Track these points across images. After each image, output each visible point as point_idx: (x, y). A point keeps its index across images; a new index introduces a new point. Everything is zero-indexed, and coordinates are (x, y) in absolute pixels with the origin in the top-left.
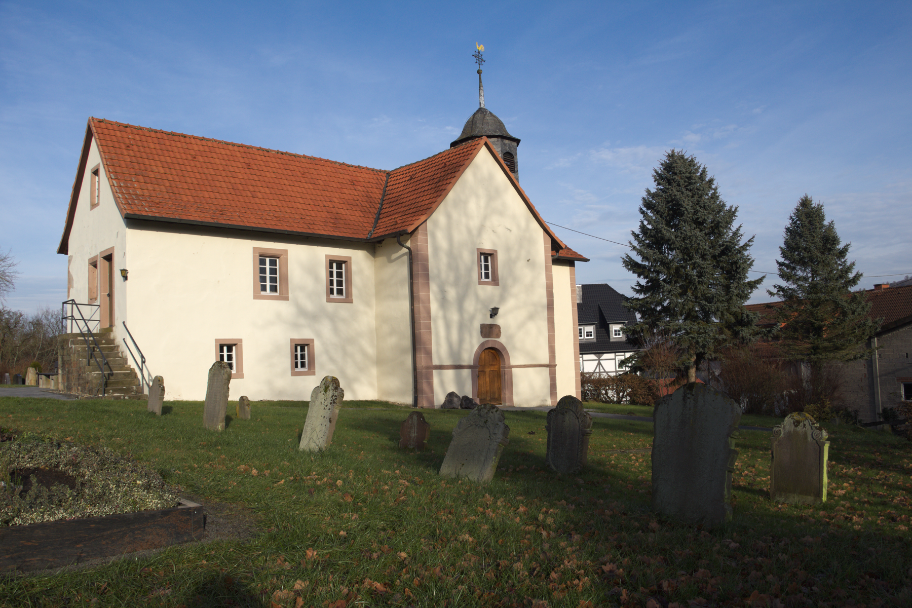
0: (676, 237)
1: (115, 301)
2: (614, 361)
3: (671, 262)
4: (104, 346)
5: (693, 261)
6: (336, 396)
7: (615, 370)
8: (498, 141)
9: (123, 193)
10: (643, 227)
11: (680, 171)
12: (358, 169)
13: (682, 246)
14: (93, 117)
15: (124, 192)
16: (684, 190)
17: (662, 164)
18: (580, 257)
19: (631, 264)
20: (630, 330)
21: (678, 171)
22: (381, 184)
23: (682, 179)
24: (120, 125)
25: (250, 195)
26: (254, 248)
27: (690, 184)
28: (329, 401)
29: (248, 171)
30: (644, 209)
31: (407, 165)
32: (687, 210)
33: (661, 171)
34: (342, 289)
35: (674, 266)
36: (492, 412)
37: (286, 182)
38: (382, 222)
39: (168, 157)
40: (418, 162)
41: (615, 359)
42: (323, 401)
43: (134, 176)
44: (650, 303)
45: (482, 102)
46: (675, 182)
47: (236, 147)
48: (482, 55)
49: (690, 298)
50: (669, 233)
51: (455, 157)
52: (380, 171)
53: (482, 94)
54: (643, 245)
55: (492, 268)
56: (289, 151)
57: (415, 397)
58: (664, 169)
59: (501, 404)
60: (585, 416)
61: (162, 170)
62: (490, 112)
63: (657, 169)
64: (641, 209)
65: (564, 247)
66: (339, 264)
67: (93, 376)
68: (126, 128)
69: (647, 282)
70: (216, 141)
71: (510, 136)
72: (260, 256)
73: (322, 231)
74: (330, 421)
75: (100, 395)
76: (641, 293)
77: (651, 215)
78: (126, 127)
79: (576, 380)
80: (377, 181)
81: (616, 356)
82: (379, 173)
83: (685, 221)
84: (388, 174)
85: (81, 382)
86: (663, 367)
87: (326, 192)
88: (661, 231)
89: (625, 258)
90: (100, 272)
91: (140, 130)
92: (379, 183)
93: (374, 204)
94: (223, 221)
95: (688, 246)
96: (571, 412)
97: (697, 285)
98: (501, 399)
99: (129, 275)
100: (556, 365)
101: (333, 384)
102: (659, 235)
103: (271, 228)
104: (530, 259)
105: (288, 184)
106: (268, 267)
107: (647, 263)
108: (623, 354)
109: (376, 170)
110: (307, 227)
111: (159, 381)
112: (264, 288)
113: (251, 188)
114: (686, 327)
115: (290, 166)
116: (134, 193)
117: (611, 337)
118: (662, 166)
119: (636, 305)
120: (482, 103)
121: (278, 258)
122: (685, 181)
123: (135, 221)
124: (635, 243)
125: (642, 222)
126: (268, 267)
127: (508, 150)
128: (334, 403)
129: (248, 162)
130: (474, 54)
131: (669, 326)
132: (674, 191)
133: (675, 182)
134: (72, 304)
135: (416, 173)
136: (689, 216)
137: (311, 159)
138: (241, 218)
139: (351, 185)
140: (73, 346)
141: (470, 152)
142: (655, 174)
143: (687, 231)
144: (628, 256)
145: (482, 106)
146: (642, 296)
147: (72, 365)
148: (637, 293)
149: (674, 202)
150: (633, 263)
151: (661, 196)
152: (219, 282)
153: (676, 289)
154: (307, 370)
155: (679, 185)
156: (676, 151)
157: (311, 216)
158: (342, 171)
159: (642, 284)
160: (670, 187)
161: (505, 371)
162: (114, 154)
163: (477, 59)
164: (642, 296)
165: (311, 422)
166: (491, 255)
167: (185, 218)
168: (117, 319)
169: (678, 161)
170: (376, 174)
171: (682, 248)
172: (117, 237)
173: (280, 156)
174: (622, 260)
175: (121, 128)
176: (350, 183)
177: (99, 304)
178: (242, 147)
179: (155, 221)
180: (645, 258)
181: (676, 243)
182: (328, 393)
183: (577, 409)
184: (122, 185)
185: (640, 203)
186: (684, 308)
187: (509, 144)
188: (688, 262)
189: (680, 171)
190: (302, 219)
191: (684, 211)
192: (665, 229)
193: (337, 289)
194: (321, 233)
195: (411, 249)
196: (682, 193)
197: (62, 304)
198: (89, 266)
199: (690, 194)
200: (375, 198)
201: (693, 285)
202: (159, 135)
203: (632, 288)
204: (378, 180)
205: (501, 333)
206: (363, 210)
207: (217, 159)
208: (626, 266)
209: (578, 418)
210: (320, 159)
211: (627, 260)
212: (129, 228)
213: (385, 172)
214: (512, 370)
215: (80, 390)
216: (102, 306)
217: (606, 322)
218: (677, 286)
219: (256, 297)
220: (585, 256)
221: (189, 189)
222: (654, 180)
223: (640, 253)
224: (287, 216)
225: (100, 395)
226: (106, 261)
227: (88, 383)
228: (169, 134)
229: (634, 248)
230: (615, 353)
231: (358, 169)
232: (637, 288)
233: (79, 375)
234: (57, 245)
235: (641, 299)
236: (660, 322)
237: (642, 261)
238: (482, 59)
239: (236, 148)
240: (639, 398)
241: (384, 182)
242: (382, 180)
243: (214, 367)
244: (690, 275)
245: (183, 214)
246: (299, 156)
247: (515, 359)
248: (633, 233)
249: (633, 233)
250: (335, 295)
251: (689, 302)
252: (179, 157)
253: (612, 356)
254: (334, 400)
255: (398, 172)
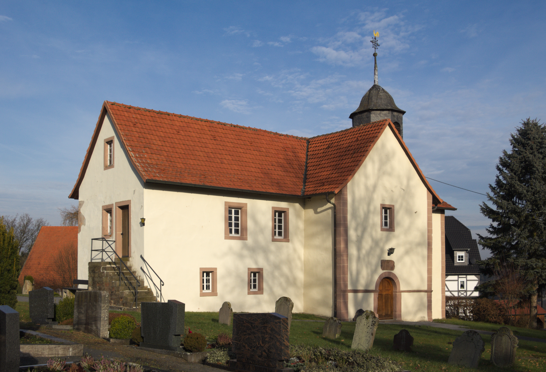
0: (527, 191)
1: (132, 239)
2: (457, 282)
3: (522, 211)
4: (125, 271)
5: (540, 211)
6: (375, 321)
7: (457, 290)
8: (389, 113)
9: (139, 162)
10: (498, 182)
11: (534, 138)
12: (286, 137)
13: (532, 199)
14: (107, 101)
15: (140, 161)
16: (536, 153)
17: (518, 130)
18: (449, 207)
19: (487, 211)
20: (485, 263)
21: (532, 137)
22: (304, 150)
23: (534, 143)
24: (125, 106)
25: (219, 162)
26: (226, 202)
27: (541, 148)
28: (370, 324)
29: (214, 142)
30: (500, 167)
31: (323, 135)
32: (538, 170)
33: (517, 136)
34: (238, 217)
35: (524, 215)
36: (475, 335)
37: (241, 150)
38: (309, 182)
39: (161, 132)
40: (333, 133)
41: (458, 280)
42: (366, 324)
43: (143, 148)
44: (502, 242)
45: (376, 80)
46: (528, 146)
47: (203, 122)
48: (377, 41)
49: (537, 240)
50: (521, 188)
51: (366, 134)
52: (302, 138)
53: (377, 73)
54: (499, 196)
55: (390, 218)
56: (239, 124)
57: (335, 312)
58: (520, 134)
59: (392, 319)
60: (514, 338)
61: (160, 143)
62: (382, 88)
63: (514, 134)
64: (498, 167)
65: (441, 202)
66: (280, 214)
67: (126, 294)
68: (129, 109)
69: (499, 225)
70: (190, 117)
71: (400, 109)
72: (229, 208)
73: (271, 190)
74: (372, 335)
75: (134, 307)
76: (494, 234)
77: (506, 171)
78: (130, 108)
79: (442, 301)
80: (300, 147)
81: (459, 278)
82: (301, 140)
83: (535, 178)
84: (308, 141)
85: (114, 297)
86: (512, 294)
87: (268, 157)
88: (514, 186)
89: (483, 206)
90: (116, 217)
91: (139, 111)
92: (302, 149)
93: (301, 166)
94: (208, 183)
95: (537, 199)
96: (506, 336)
97: (543, 230)
98: (392, 315)
99: (145, 222)
100: (432, 291)
101: (372, 315)
102: (513, 189)
103: (239, 188)
104: (417, 212)
105: (243, 152)
106: (233, 216)
107: (501, 211)
108: (465, 276)
109: (299, 138)
110: (261, 187)
111: (229, 305)
112: (231, 231)
113: (219, 156)
114: (532, 264)
115: (242, 137)
116: (146, 162)
117: (455, 262)
118: (518, 132)
119: (490, 243)
120: (376, 80)
121: (240, 209)
122: (537, 145)
123: (150, 184)
124: (492, 194)
125: (498, 177)
126: (233, 216)
127: (396, 120)
128: (374, 325)
129: (213, 135)
130: (372, 40)
131: (518, 262)
132: (528, 154)
133: (528, 146)
134: (103, 240)
135: (332, 143)
136: (539, 174)
137: (254, 130)
138: (218, 180)
139: (284, 151)
140: (105, 272)
141: (378, 131)
142: (512, 139)
143: (537, 187)
144: (485, 204)
145: (376, 83)
146: (494, 236)
147: (104, 284)
148: (491, 234)
149: (527, 163)
150: (489, 210)
151: (516, 157)
152: (202, 227)
153: (525, 233)
154: (257, 290)
155: (532, 149)
156: (531, 119)
157: (261, 177)
158: (276, 140)
159: (495, 227)
160: (524, 150)
161: (396, 294)
162: (127, 131)
163: (374, 44)
164: (494, 236)
165: (359, 335)
166: (389, 208)
167: (183, 181)
168: (134, 253)
169: (532, 129)
170: (300, 141)
171: (531, 201)
172: (134, 194)
173: (233, 128)
174: (480, 207)
175: (128, 109)
176: (283, 150)
177: (114, 240)
178: (207, 122)
179: (166, 184)
180: (499, 206)
181: (527, 196)
182: (369, 319)
183: (510, 334)
184: (137, 156)
185: (497, 161)
186: (531, 248)
187: (397, 116)
188: (537, 212)
189: (534, 138)
190: (256, 180)
191: (535, 171)
192: (518, 185)
193: (235, 217)
194: (271, 192)
195: (336, 204)
196: (535, 156)
197: (91, 240)
198: (102, 211)
199: (541, 156)
200: (301, 161)
201: (539, 231)
202: (152, 114)
203: (487, 230)
204: (301, 146)
205: (394, 266)
206: (294, 172)
207: (193, 133)
208: (484, 212)
209: (510, 339)
210: (260, 130)
211: (484, 207)
212: (146, 188)
213: (305, 139)
214: (401, 294)
215: (113, 303)
216: (117, 241)
217: (452, 249)
218: (526, 231)
219: (227, 238)
220: (454, 206)
221: (179, 158)
222: (510, 143)
223: (495, 202)
224: (246, 178)
225: (134, 307)
226: (120, 209)
227: (121, 298)
228: (158, 113)
229: (491, 199)
230: (458, 275)
231: (286, 137)
232: (491, 229)
233: (112, 292)
234: (70, 192)
235: (494, 239)
236: (510, 258)
237: (497, 209)
238: (377, 44)
239: (203, 123)
240: (492, 317)
241: (306, 148)
242: (304, 146)
243: (280, 300)
244: (538, 223)
245: (181, 178)
246: (246, 128)
247: (402, 287)
248: (491, 186)
249: (491, 186)
250: (277, 237)
251: (535, 244)
252: (168, 132)
253: (455, 277)
254: (374, 324)
255: (317, 140)
